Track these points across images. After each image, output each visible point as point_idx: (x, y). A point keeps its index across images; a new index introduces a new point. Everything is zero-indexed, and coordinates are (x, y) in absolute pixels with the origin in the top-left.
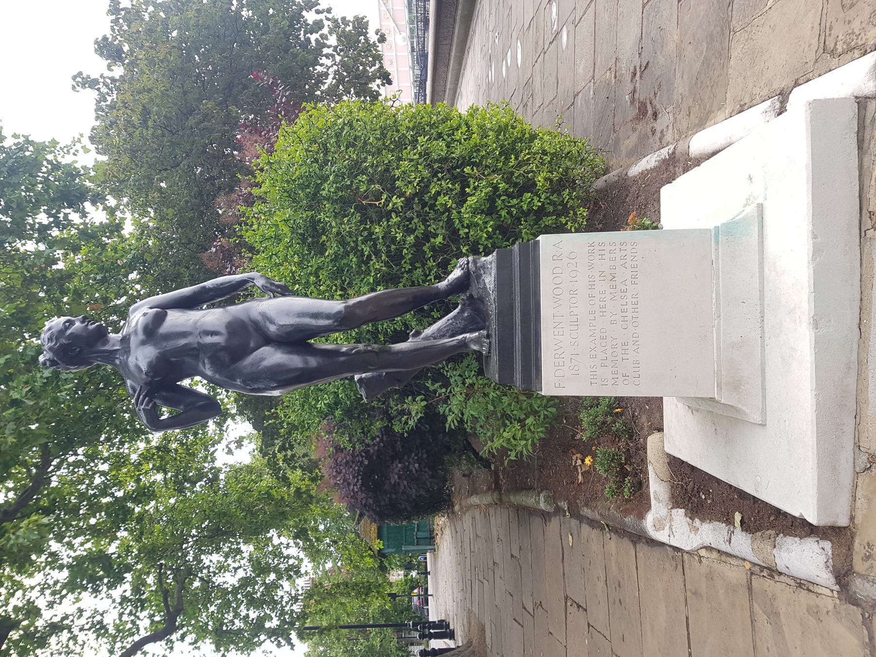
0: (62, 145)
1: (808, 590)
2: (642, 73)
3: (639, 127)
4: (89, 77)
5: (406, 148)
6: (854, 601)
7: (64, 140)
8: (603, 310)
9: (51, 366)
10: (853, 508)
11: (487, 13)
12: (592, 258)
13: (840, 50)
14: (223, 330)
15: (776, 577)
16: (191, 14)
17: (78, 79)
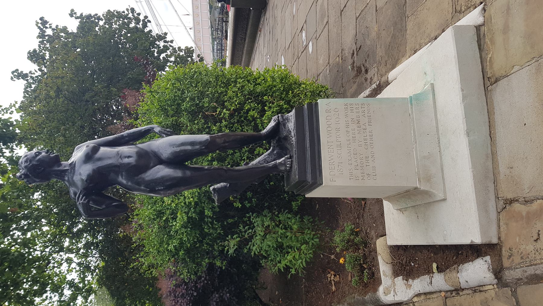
0: (3, 108)
1: (480, 291)
2: (357, 52)
3: (357, 80)
4: (22, 72)
5: (231, 85)
6: (506, 285)
9: (25, 178)
10: (499, 232)
11: (262, 47)
13: (463, 9)
14: (135, 155)
15: (461, 293)
16: (91, 39)
17: (15, 74)
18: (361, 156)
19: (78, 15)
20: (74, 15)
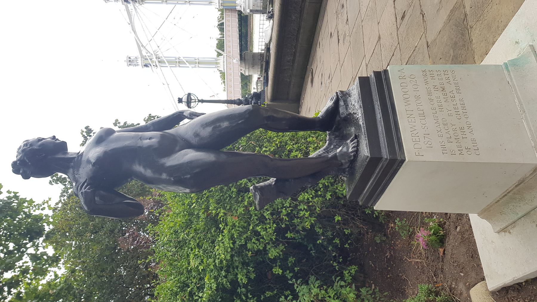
0: (35, 204)
7: (38, 201)
18: (454, 127)
19: (122, 124)
20: (118, 125)
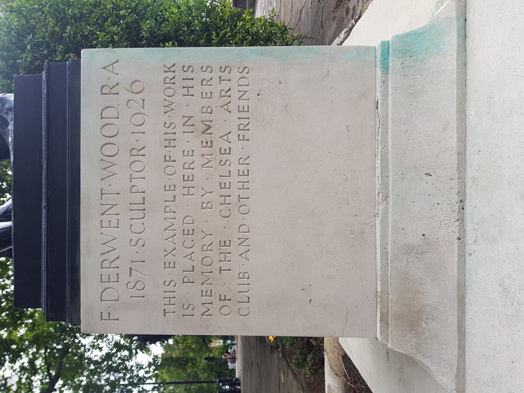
8: (190, 184)
12: (170, 92)
